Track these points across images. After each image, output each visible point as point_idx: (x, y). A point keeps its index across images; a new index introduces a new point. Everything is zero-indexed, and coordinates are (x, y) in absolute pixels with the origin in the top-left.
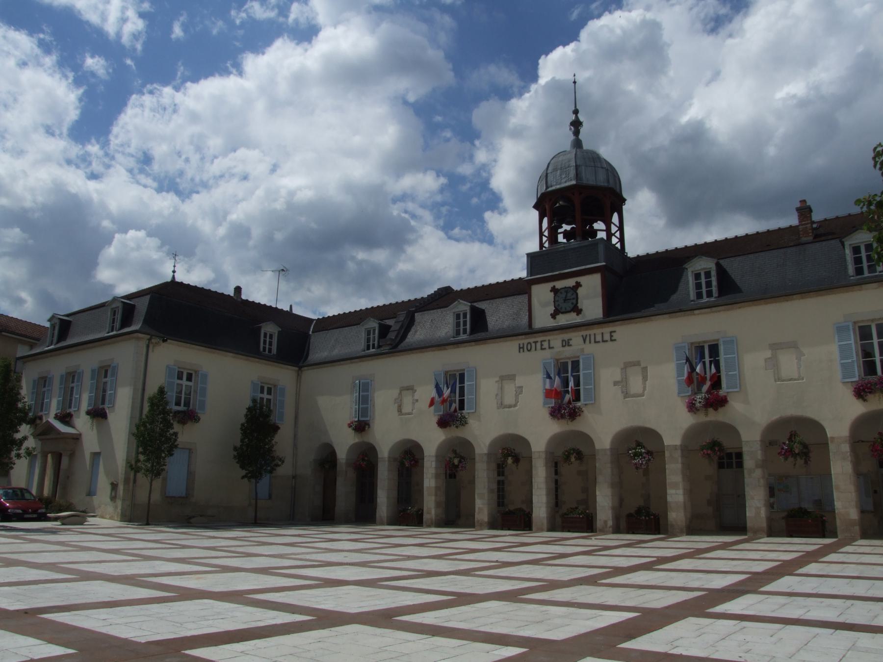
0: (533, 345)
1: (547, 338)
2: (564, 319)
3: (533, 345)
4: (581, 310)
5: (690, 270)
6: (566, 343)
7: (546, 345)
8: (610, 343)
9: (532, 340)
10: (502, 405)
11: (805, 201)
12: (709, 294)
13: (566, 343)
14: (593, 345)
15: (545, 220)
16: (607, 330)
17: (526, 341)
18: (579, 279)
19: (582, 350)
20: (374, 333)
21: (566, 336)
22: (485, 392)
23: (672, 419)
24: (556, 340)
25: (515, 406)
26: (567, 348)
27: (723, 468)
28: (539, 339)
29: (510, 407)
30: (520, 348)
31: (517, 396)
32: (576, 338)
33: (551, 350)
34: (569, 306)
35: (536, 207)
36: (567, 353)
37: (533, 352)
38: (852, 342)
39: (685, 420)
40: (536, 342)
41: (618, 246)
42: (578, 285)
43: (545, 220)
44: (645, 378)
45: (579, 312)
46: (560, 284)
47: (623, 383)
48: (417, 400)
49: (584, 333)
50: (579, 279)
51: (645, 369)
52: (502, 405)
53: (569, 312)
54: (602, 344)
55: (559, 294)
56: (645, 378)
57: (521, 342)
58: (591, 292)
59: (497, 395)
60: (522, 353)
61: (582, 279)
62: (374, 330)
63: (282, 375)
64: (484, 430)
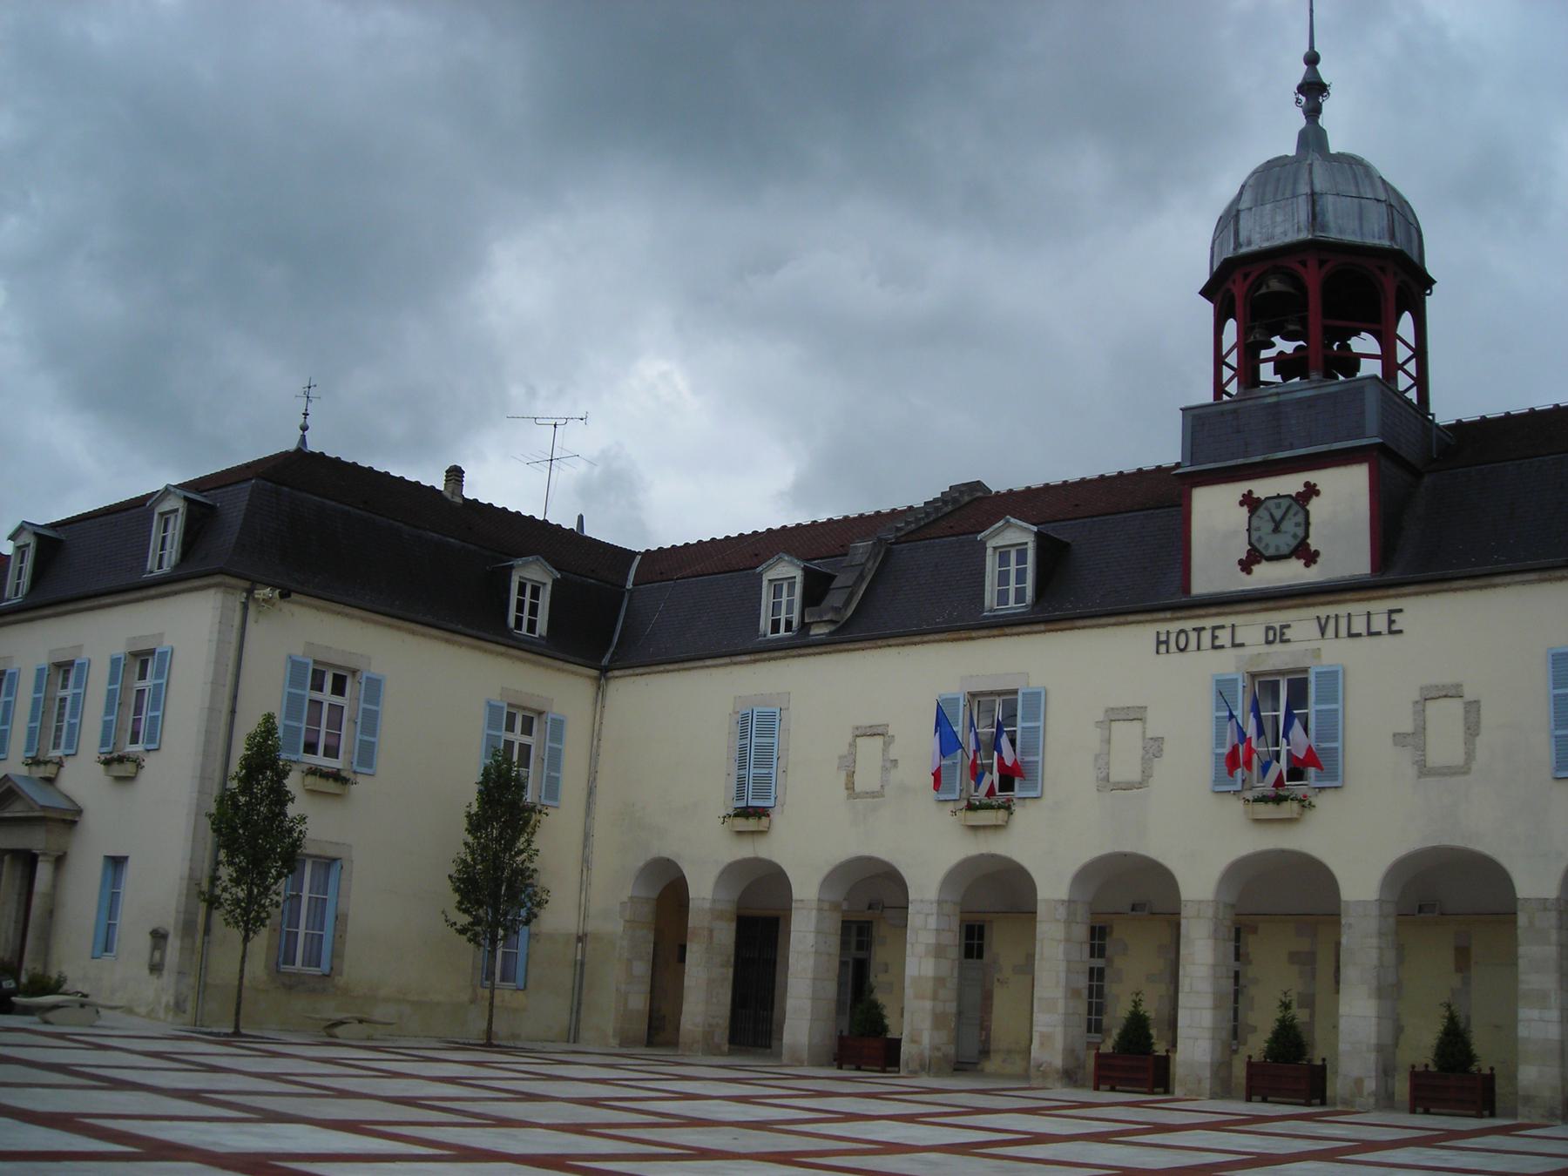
0: (1193, 636)
1: (1227, 621)
2: (1268, 575)
3: (1193, 636)
4: (1317, 553)
6: (1276, 636)
7: (1224, 637)
8: (1387, 640)
9: (1189, 625)
14: (1346, 643)
15: (1231, 326)
16: (1379, 607)
17: (1174, 627)
19: (1317, 653)
21: (1277, 618)
22: (1065, 747)
24: (1251, 627)
26: (1277, 647)
28: (1208, 623)
30: (1159, 643)
32: (1302, 623)
33: (1240, 651)
34: (1285, 541)
36: (1279, 658)
37: (1192, 655)
40: (1199, 630)
41: (1412, 395)
42: (1311, 491)
43: (1231, 326)
44: (1472, 729)
45: (1310, 558)
46: (1263, 488)
49: (1323, 611)
54: (1366, 641)
55: (1261, 512)
56: (1472, 729)
57: (1163, 628)
60: (1163, 657)
63: (562, 691)
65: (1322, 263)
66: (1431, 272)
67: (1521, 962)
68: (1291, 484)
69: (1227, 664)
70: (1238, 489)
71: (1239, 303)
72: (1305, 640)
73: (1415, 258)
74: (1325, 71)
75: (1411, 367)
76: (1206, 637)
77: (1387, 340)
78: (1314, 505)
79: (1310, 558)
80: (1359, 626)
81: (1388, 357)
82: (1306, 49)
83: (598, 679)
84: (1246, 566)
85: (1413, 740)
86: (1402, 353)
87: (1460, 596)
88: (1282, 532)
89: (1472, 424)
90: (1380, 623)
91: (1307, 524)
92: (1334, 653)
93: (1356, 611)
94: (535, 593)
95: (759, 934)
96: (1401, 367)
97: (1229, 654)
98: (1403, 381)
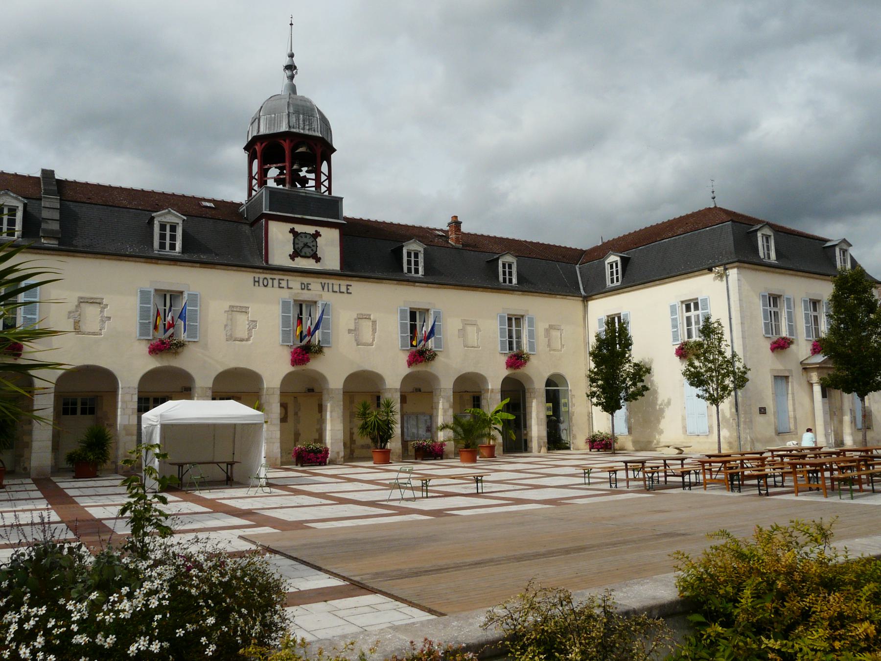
0: (270, 282)
1: (285, 278)
2: (302, 263)
3: (270, 282)
5: (606, 262)
6: (305, 287)
7: (284, 284)
8: (346, 295)
9: (269, 276)
10: (231, 338)
11: (456, 217)
12: (617, 281)
13: (305, 287)
14: (331, 293)
15: (256, 162)
16: (344, 283)
17: (262, 276)
18: (319, 229)
19: (321, 296)
20: (617, 267)
21: (306, 280)
23: (393, 368)
24: (295, 282)
25: (248, 340)
26: (305, 291)
27: (74, 412)
28: (277, 277)
29: (242, 340)
30: (255, 281)
31: (250, 330)
32: (315, 284)
33: (290, 290)
35: (246, 149)
36: (306, 295)
37: (269, 289)
38: (291, 315)
39: (504, 372)
40: (273, 279)
42: (317, 234)
43: (256, 162)
44: (374, 331)
45: (318, 260)
46: (299, 228)
47: (354, 331)
48: (109, 318)
49: (323, 281)
50: (321, 230)
51: (374, 322)
52: (231, 338)
53: (308, 257)
54: (339, 294)
55: (312, 239)
56: (374, 331)
57: (257, 276)
58: (329, 244)
59: (226, 326)
60: (257, 288)
61: (322, 230)
62: (617, 264)
64: (448, 367)
65: (292, 141)
66: (335, 146)
67: (136, 400)
68: (311, 230)
69: (285, 294)
70: (289, 226)
71: (258, 155)
72: (316, 289)
73: (329, 141)
74: (296, 61)
75: (326, 183)
76: (276, 282)
77: (318, 173)
78: (319, 239)
79: (318, 260)
80: (336, 288)
81: (318, 180)
82: (289, 51)
83: (583, 301)
84: (292, 257)
85: (354, 331)
86: (323, 178)
87: (245, 274)
88: (304, 247)
89: (227, 202)
90: (344, 289)
91: (294, 243)
92: (327, 297)
93: (335, 283)
94: (416, 255)
95: (515, 394)
96: (322, 183)
97: (286, 291)
98: (323, 189)
